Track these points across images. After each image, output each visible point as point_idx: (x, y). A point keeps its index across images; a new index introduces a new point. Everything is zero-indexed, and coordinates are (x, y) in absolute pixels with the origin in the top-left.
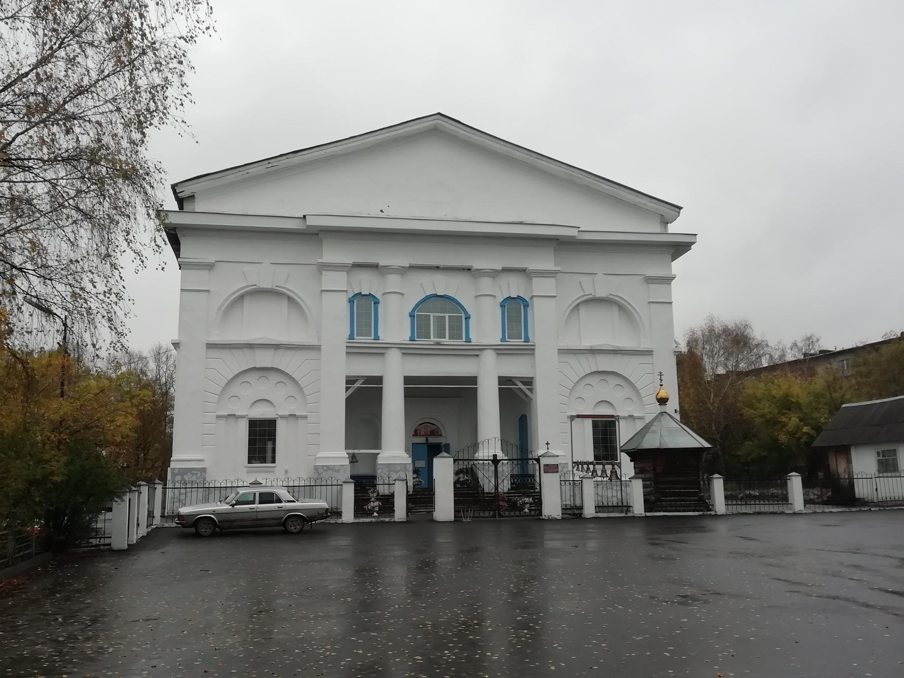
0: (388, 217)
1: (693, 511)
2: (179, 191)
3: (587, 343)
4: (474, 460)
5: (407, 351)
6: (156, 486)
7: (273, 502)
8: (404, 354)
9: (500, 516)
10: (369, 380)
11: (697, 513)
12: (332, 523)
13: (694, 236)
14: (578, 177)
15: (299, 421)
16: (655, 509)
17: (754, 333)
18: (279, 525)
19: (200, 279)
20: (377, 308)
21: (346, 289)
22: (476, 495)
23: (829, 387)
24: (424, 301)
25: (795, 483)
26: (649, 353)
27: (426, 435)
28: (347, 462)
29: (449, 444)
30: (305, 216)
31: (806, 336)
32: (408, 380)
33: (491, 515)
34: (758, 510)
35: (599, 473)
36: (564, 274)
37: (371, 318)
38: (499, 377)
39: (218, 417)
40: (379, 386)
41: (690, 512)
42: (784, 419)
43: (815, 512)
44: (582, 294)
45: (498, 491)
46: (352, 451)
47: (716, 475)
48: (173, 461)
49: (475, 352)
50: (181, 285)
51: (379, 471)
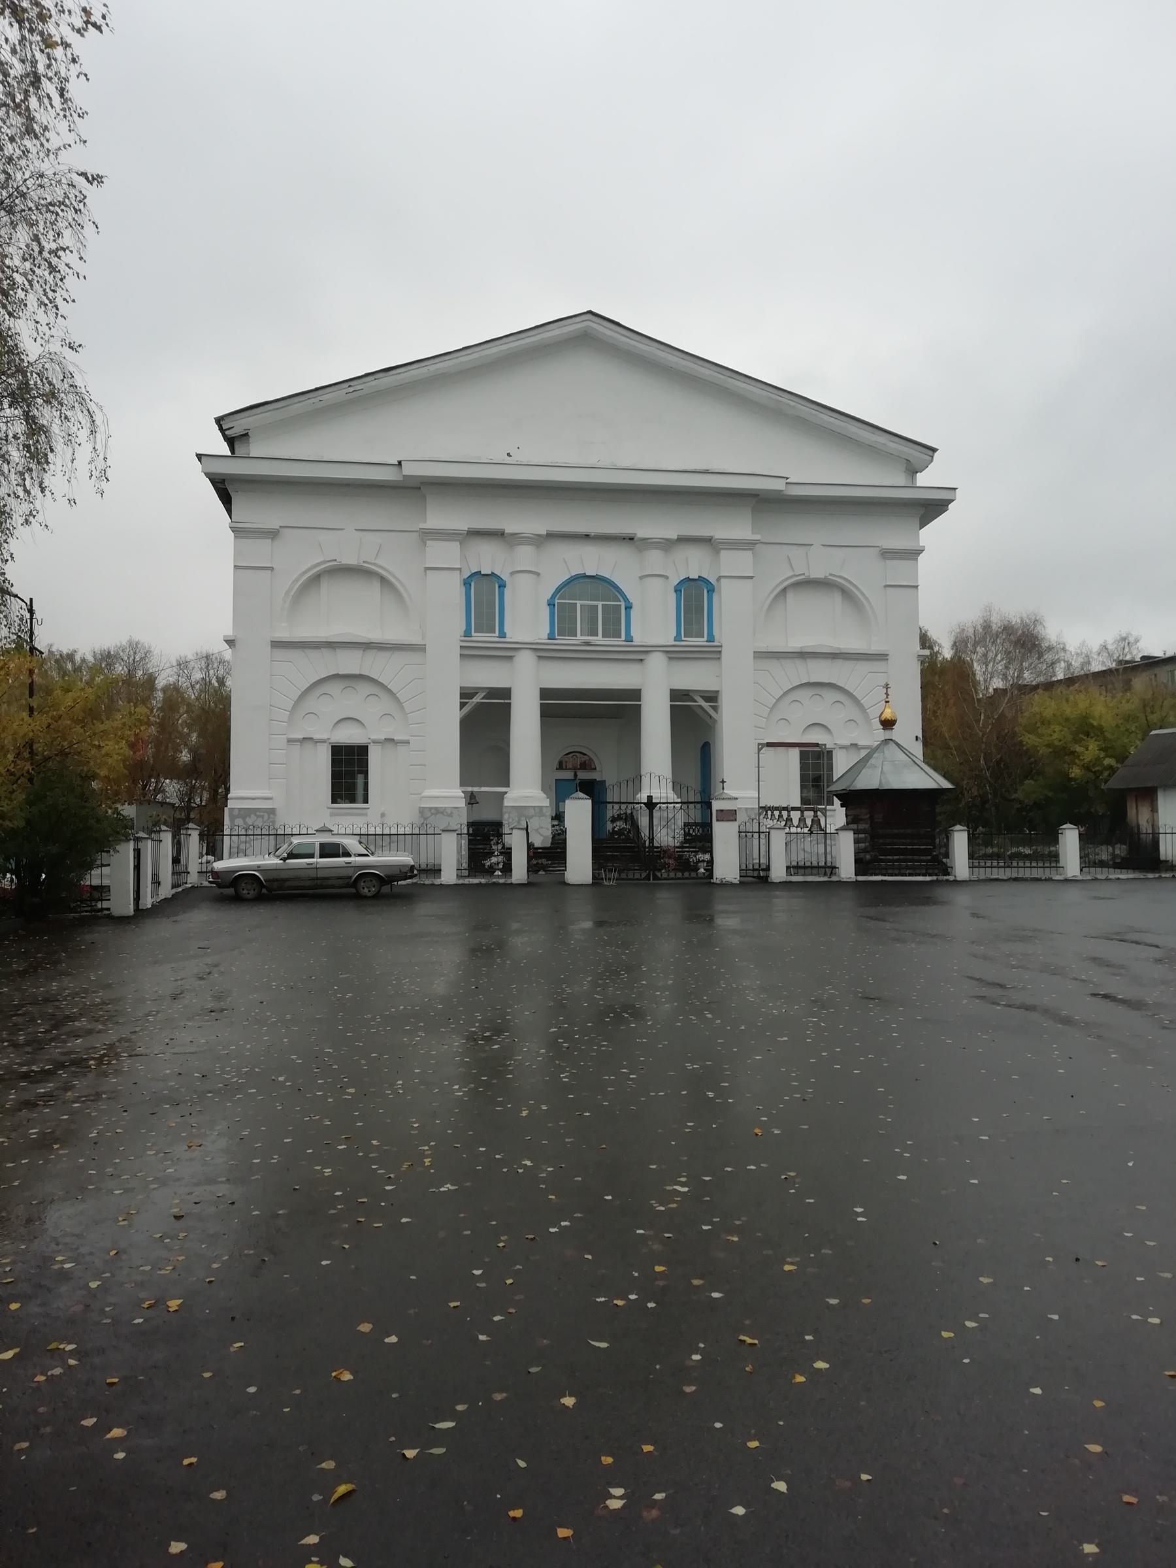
0: (517, 463)
1: (924, 875)
2: (227, 427)
3: (796, 643)
4: (634, 803)
5: (544, 654)
6: (190, 832)
7: (338, 856)
8: (540, 657)
9: (655, 878)
10: (493, 693)
11: (928, 878)
12: (428, 885)
13: (953, 491)
14: (788, 405)
15: (398, 747)
16: (871, 872)
17: (1047, 631)
18: (348, 886)
19: (260, 551)
20: (503, 593)
21: (459, 566)
22: (637, 850)
23: (1145, 706)
24: (566, 585)
25: (1070, 839)
26: (882, 657)
27: (575, 769)
28: (462, 804)
29: (605, 781)
30: (400, 463)
31: (1120, 635)
32: (545, 693)
33: (643, 877)
34: (1015, 875)
35: (796, 822)
36: (764, 546)
37: (495, 607)
38: (671, 690)
39: (289, 741)
40: (506, 701)
41: (919, 875)
42: (1078, 749)
43: (1096, 879)
44: (791, 573)
45: (653, 844)
46: (470, 789)
47: (958, 827)
48: (231, 799)
49: (638, 655)
50: (235, 560)
51: (506, 816)
